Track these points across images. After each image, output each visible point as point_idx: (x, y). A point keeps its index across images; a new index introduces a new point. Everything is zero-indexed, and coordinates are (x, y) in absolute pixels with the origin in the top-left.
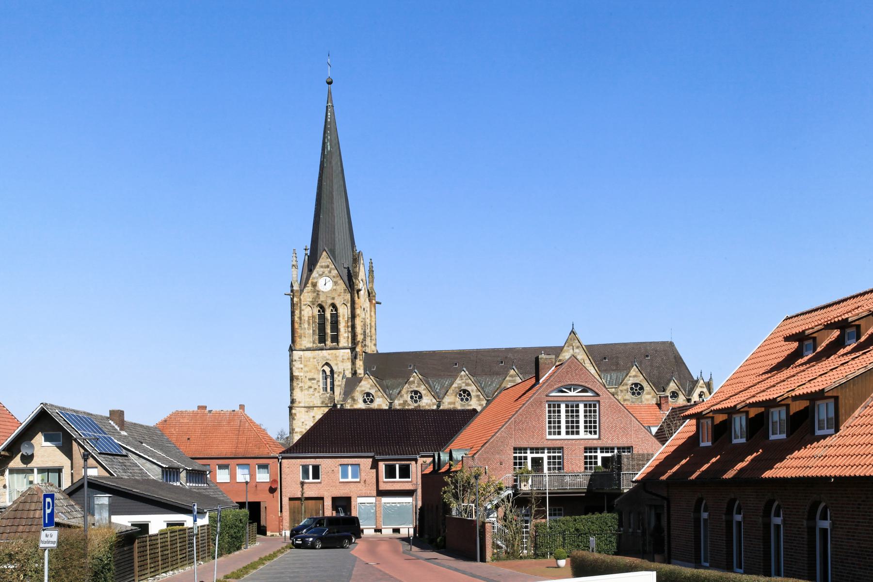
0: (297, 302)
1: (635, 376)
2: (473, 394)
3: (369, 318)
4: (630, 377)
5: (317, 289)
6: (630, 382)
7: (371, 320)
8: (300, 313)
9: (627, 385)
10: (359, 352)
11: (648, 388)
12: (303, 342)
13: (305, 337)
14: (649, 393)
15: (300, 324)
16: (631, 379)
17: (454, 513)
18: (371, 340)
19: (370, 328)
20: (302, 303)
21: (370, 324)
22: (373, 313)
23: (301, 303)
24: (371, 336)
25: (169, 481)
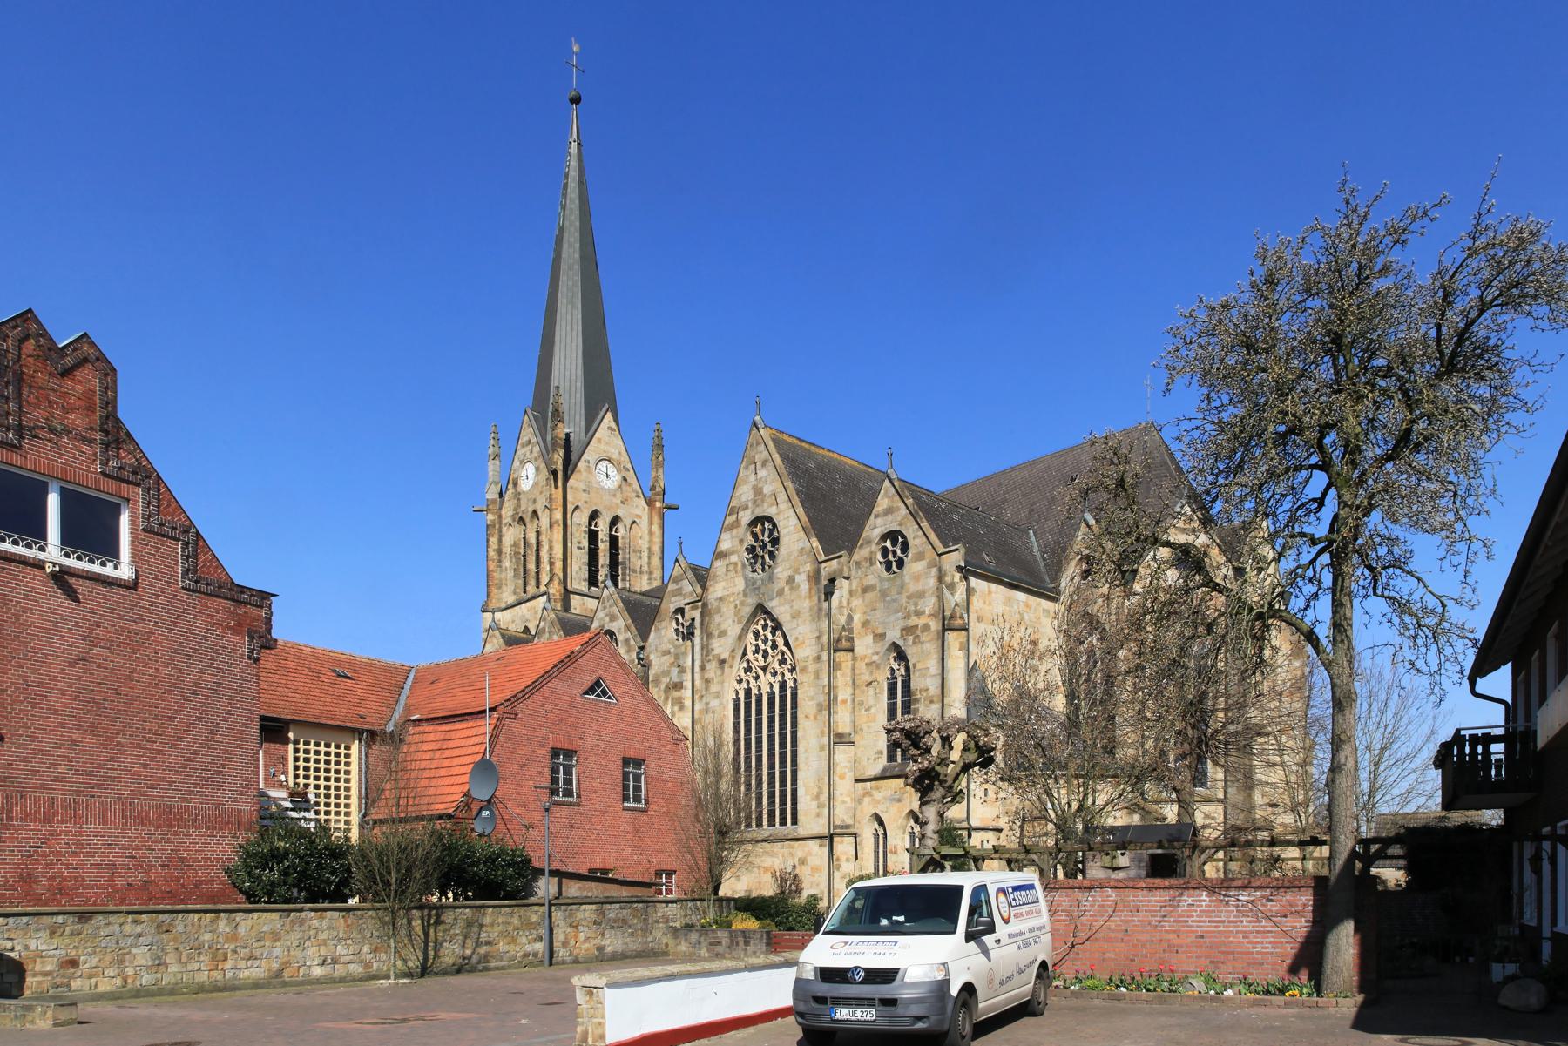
0: (493, 521)
1: (889, 511)
2: (620, 638)
3: (647, 537)
4: (876, 517)
5: (519, 490)
6: (876, 533)
7: (650, 541)
8: (500, 541)
9: (869, 542)
10: (554, 595)
11: (918, 541)
12: (504, 595)
13: (506, 585)
14: (920, 557)
15: (500, 561)
16: (879, 521)
17: (1500, 822)
18: (650, 579)
19: (649, 557)
20: (504, 522)
21: (649, 549)
22: (656, 528)
23: (500, 523)
24: (650, 573)
25: (754, 825)
